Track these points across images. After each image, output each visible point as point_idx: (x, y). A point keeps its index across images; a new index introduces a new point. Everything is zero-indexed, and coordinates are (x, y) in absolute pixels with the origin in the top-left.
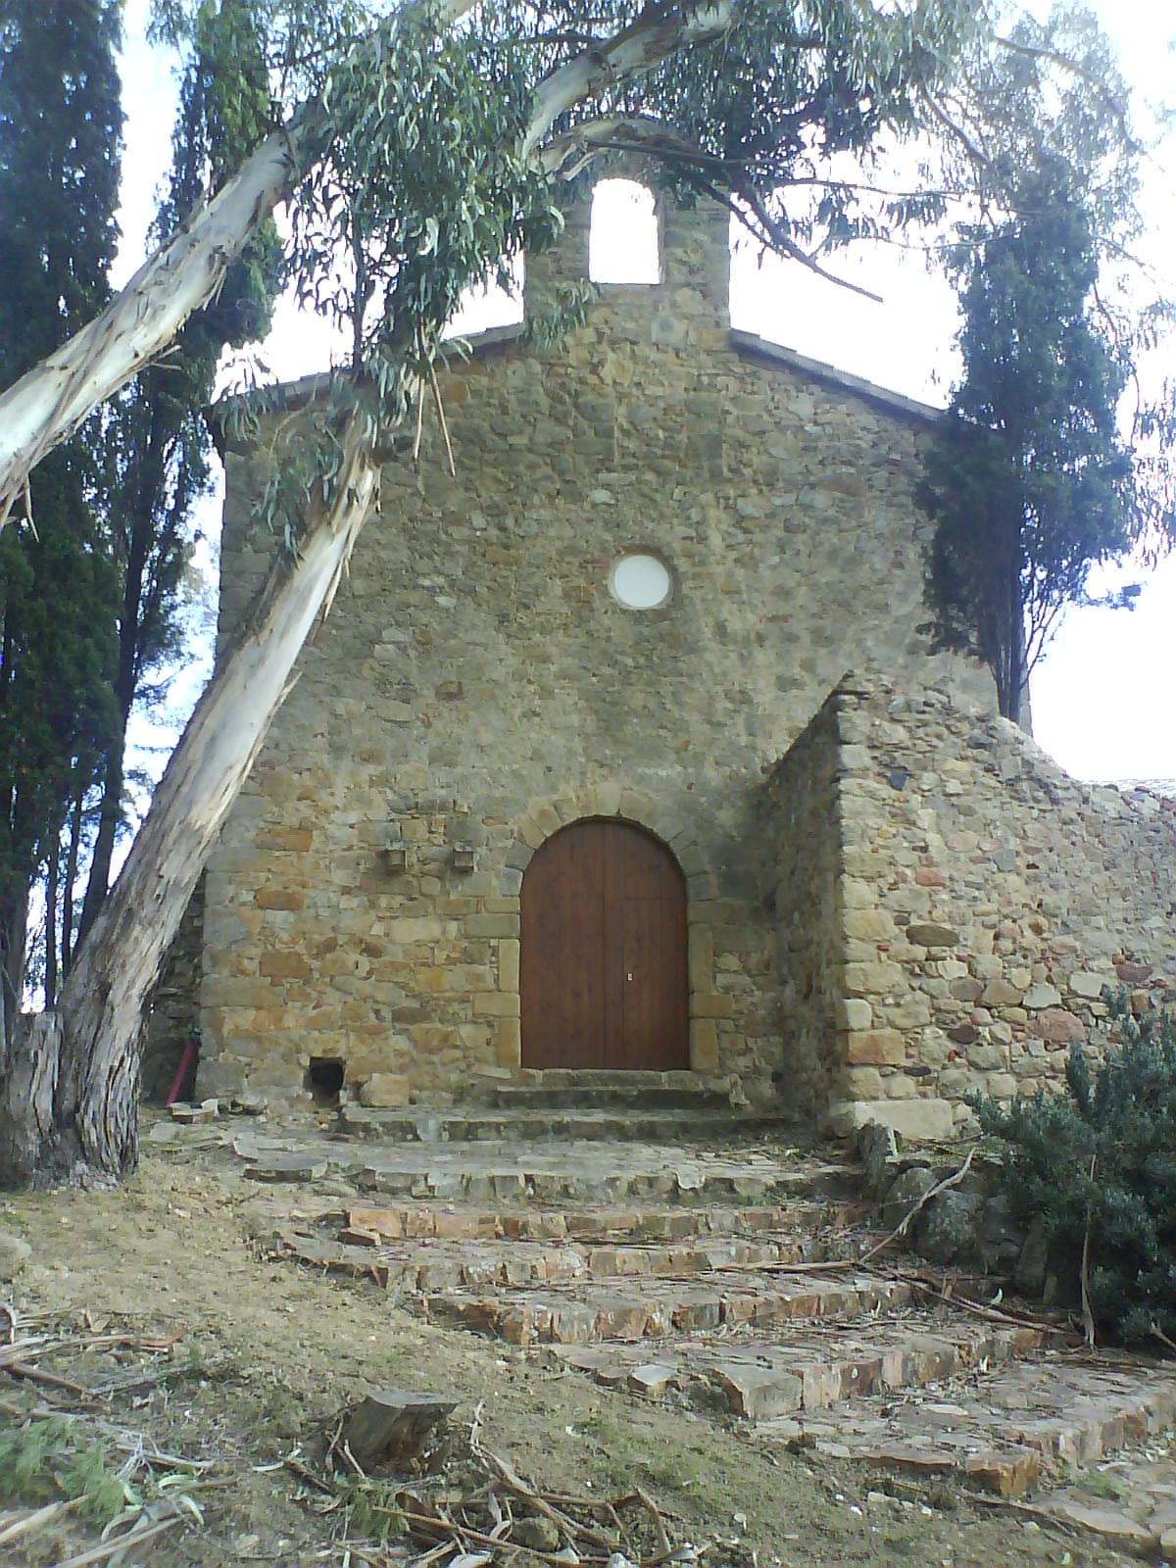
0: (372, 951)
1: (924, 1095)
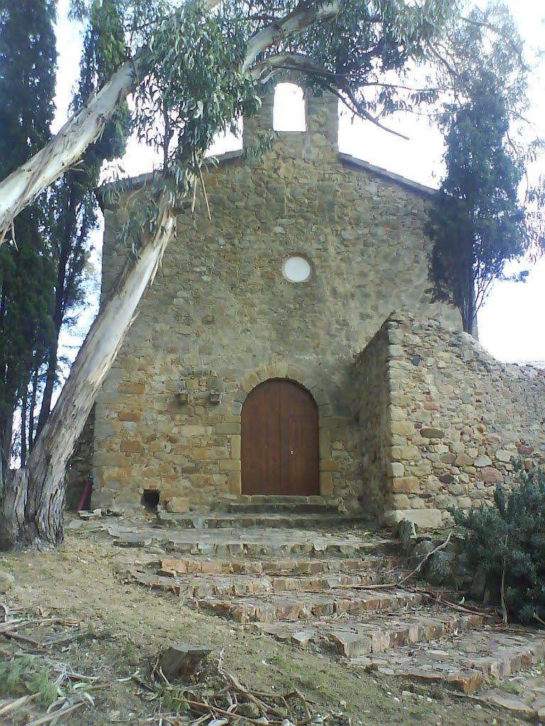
0: (172, 440)
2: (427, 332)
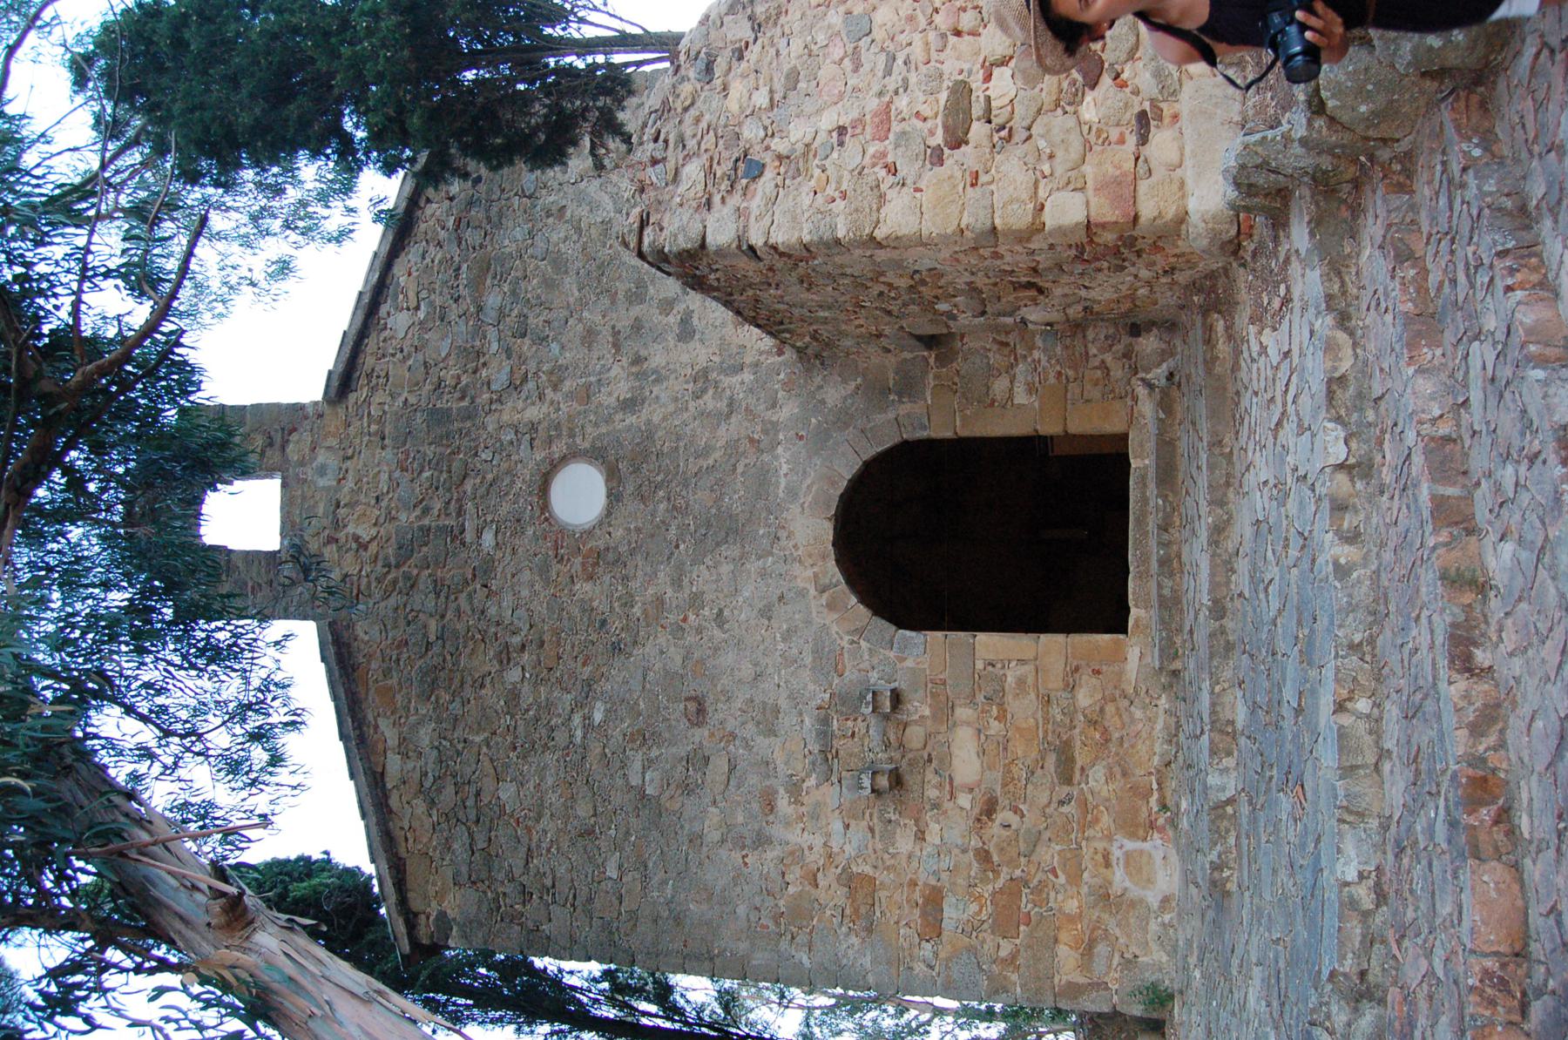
0: (990, 809)
1: (1176, 117)
2: (671, 145)
